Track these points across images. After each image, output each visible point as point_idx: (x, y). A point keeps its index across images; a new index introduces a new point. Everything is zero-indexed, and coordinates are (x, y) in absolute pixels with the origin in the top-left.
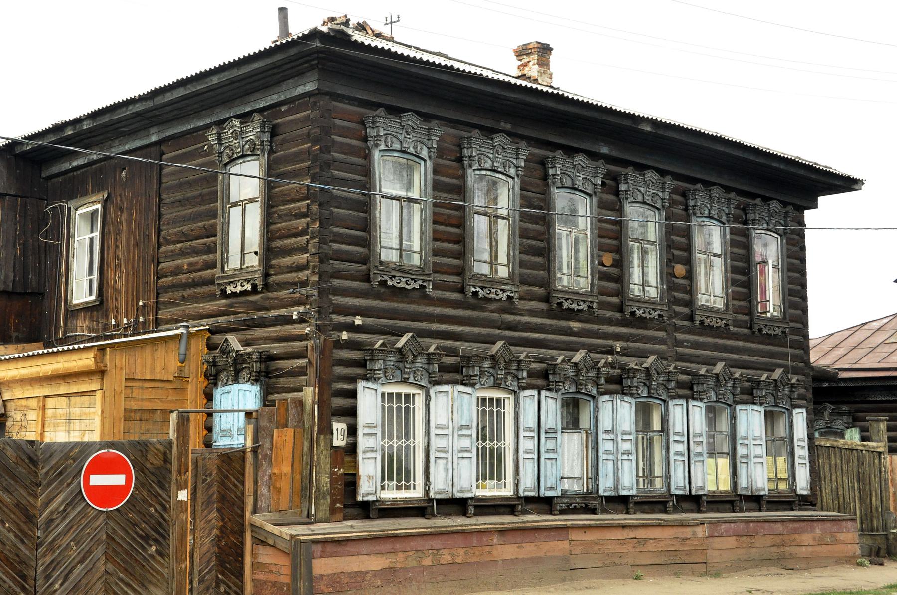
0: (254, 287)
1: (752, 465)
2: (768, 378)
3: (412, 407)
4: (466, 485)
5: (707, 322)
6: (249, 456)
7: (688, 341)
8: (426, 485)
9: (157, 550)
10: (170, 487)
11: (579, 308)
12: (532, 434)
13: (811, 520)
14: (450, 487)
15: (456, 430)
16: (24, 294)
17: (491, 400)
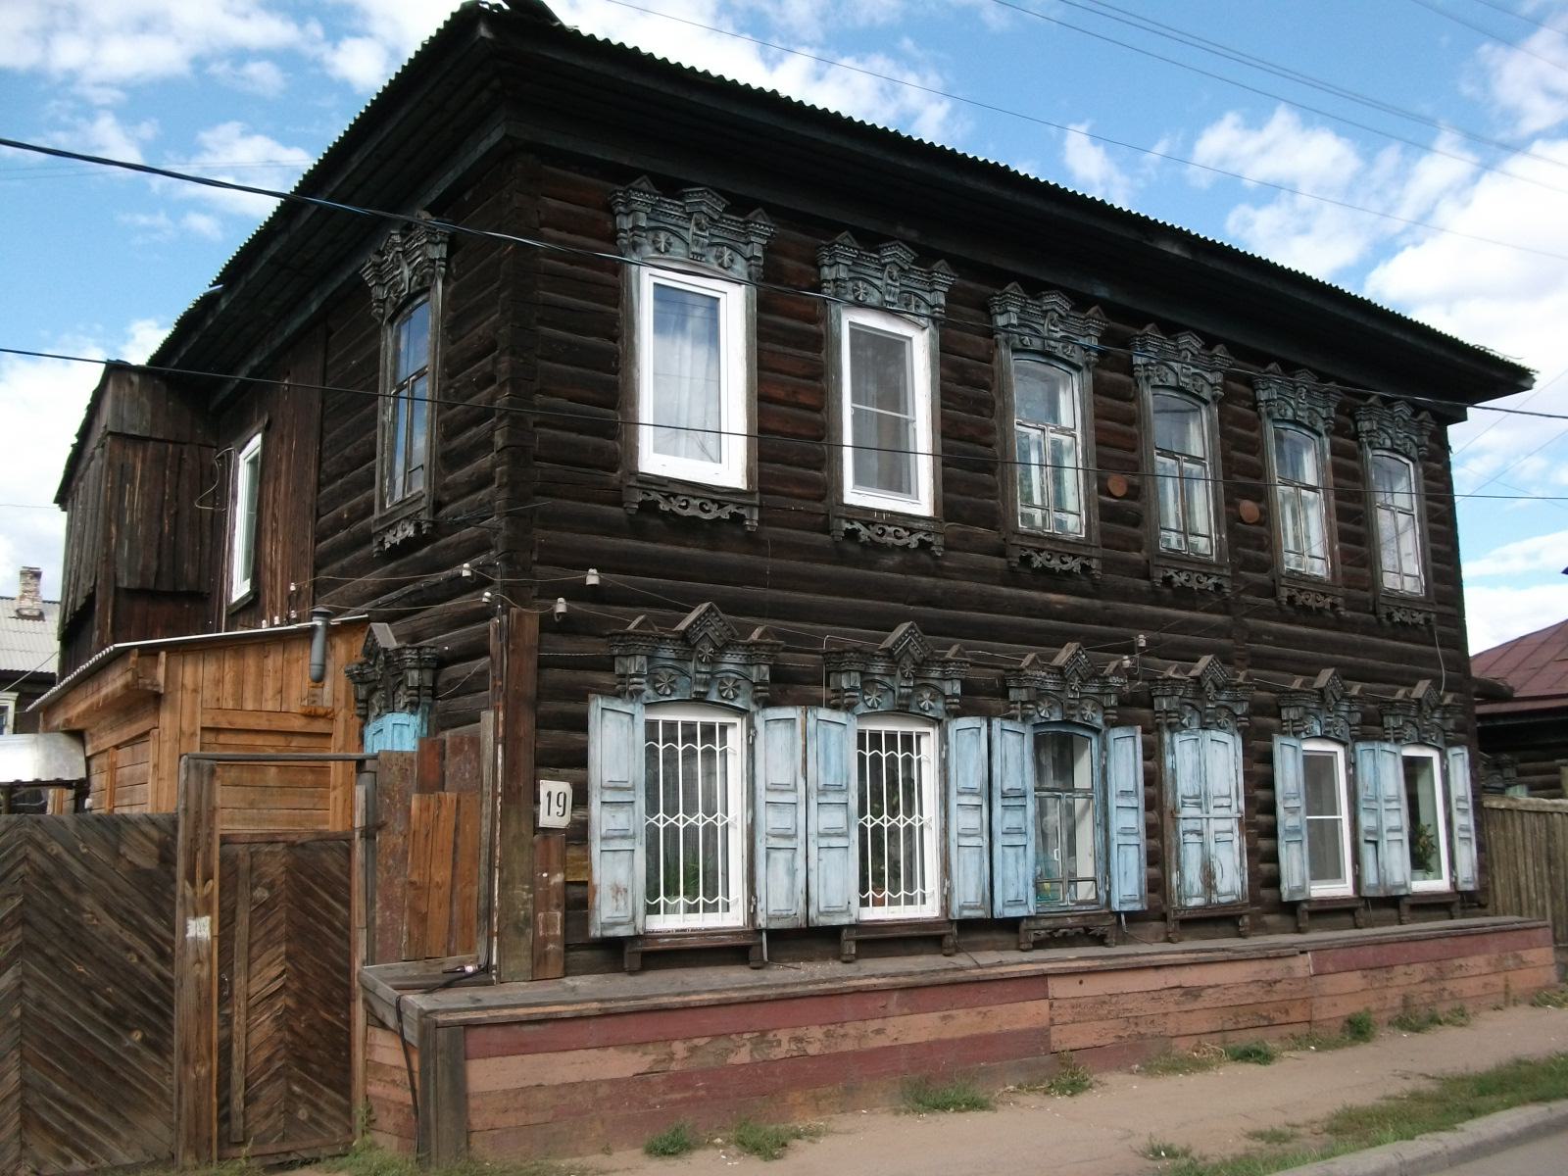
0: (418, 526)
1: (1383, 845)
2: (1406, 695)
3: (915, 758)
4: (837, 901)
5: (1301, 599)
6: (359, 846)
7: (1269, 632)
8: (750, 902)
9: (144, 1041)
10: (173, 911)
11: (1065, 567)
12: (976, 801)
13: (1480, 933)
14: (802, 904)
15: (813, 795)
16: (175, 596)
17: (891, 737)
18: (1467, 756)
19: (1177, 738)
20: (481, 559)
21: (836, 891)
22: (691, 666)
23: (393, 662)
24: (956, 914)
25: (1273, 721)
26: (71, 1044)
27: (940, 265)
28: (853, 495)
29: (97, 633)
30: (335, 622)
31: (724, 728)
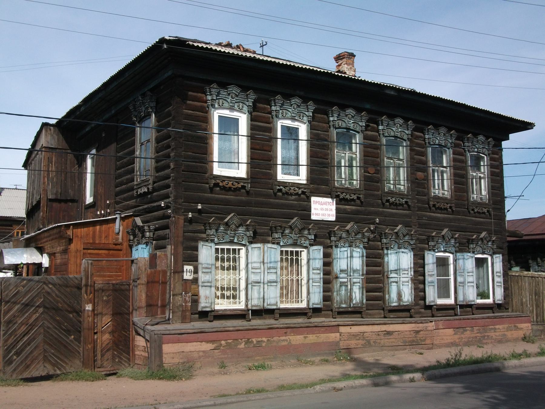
0: (148, 188)
3: (299, 258)
4: (273, 301)
11: (351, 198)
14: (262, 303)
18: (501, 258)
19: (389, 252)
20: (167, 200)
21: (273, 298)
22: (229, 232)
23: (142, 230)
24: (311, 306)
25: (427, 246)
26: (56, 339)
27: (310, 103)
28: (281, 177)
29: (42, 213)
30: (123, 216)
31: (239, 250)
